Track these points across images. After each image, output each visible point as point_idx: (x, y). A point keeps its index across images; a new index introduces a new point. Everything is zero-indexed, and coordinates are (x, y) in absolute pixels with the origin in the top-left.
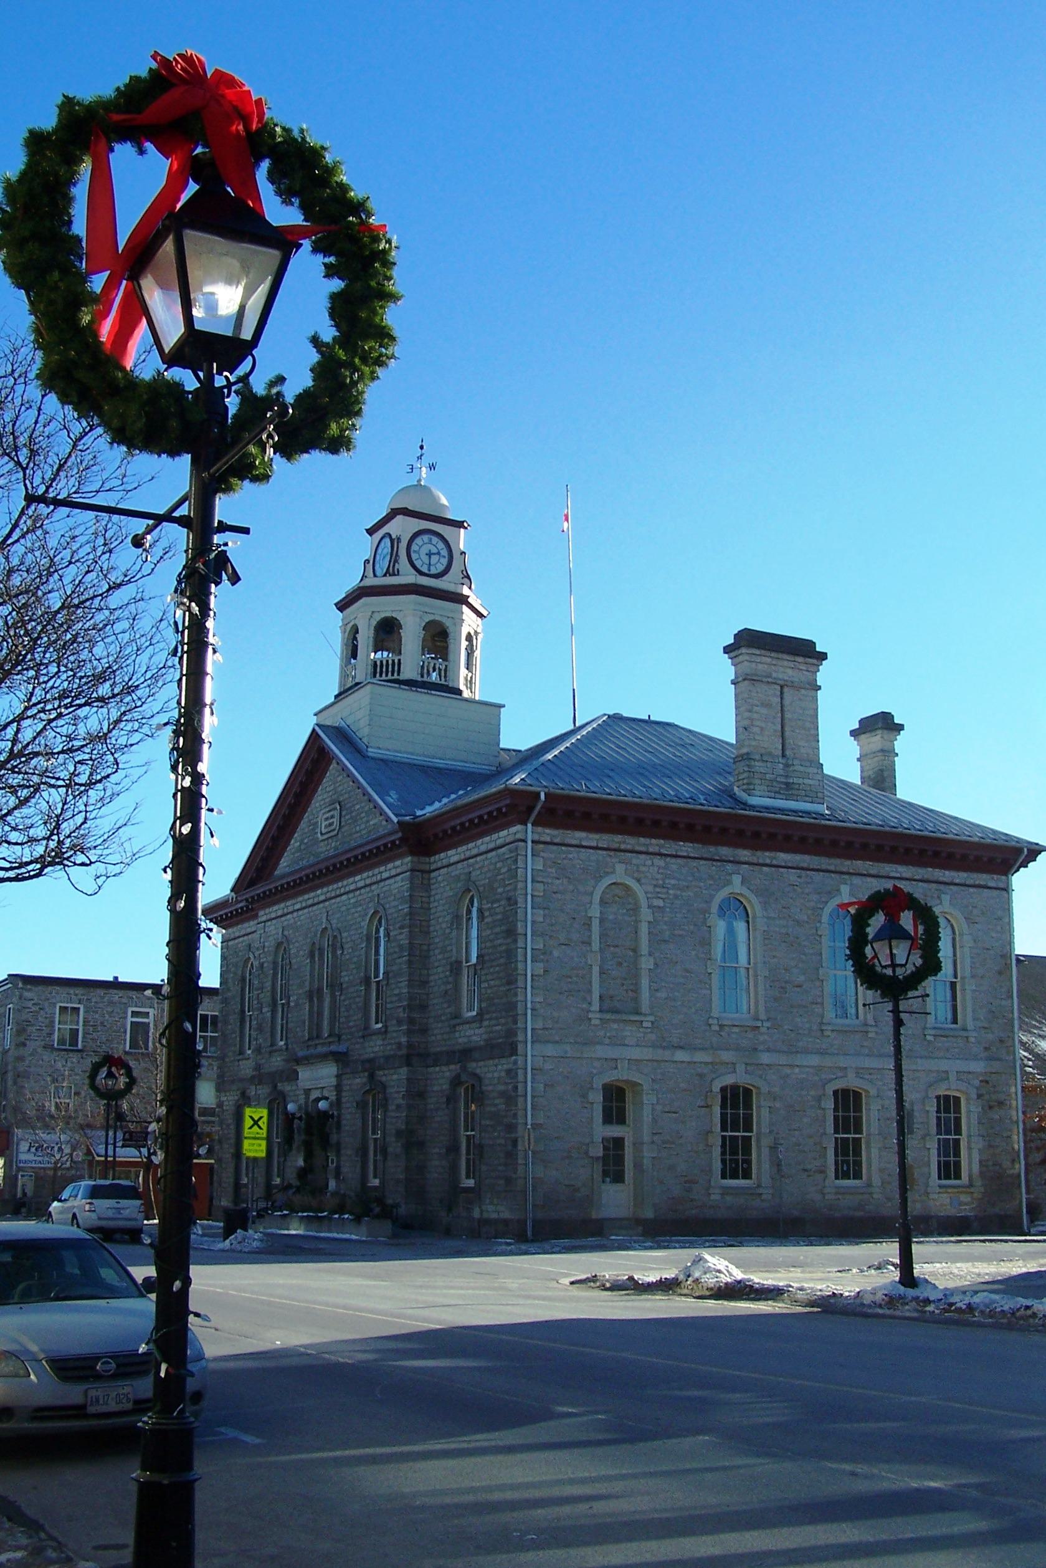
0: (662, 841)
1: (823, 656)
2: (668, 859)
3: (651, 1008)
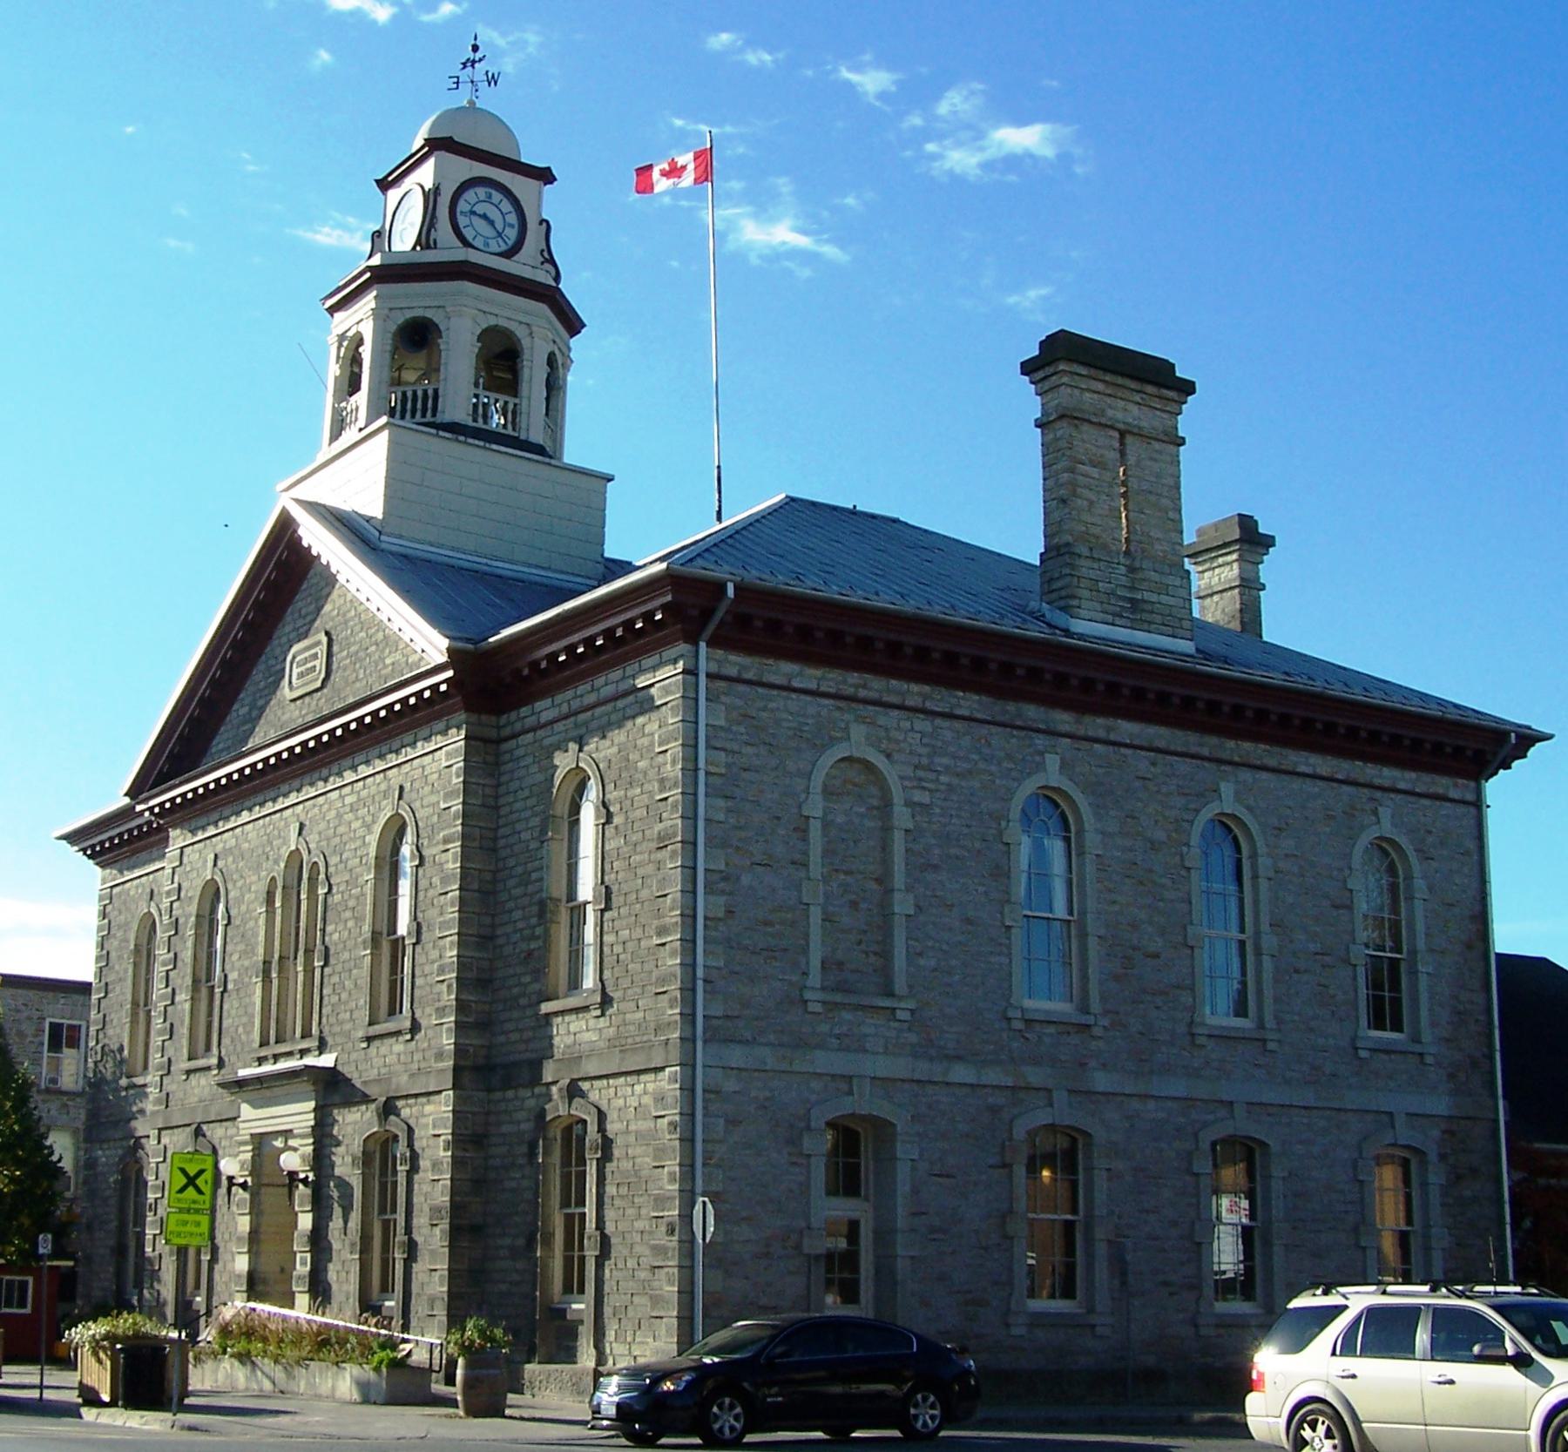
0: (927, 689)
1: (1188, 388)
2: (938, 721)
3: (911, 987)
